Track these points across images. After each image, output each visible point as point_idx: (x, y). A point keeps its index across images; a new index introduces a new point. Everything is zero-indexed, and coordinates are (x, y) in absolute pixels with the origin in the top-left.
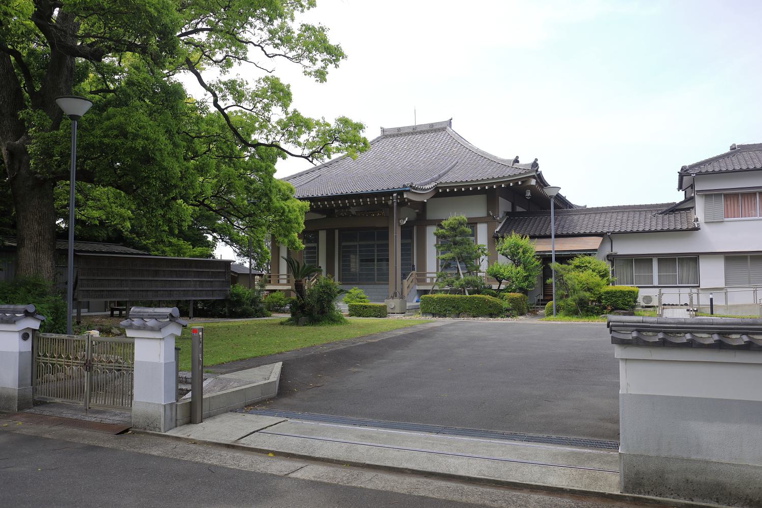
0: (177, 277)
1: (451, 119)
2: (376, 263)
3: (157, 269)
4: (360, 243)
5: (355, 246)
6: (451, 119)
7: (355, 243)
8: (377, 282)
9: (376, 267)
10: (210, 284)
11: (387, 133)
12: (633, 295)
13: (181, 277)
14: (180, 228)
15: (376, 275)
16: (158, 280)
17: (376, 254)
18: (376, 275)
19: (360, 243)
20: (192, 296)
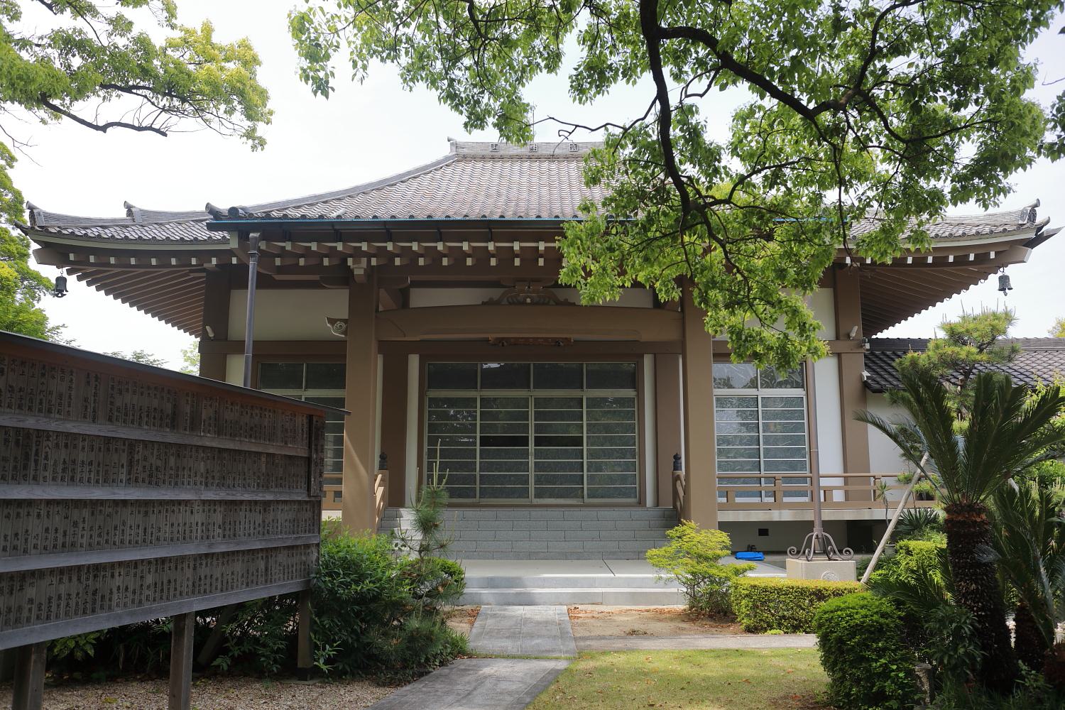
0: (132, 481)
1: (1036, 206)
2: (531, 447)
3: (30, 422)
4: (482, 393)
5: (470, 402)
6: (1036, 206)
7: (575, 393)
8: (587, 500)
9: (532, 461)
10: (259, 519)
11: (465, 151)
12: (402, 505)
13: (152, 480)
14: (648, 226)
15: (532, 480)
16: (30, 503)
17: (532, 423)
18: (532, 480)
19: (482, 393)
20: (197, 588)
